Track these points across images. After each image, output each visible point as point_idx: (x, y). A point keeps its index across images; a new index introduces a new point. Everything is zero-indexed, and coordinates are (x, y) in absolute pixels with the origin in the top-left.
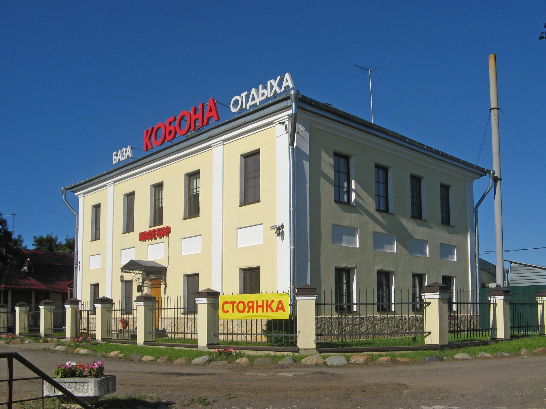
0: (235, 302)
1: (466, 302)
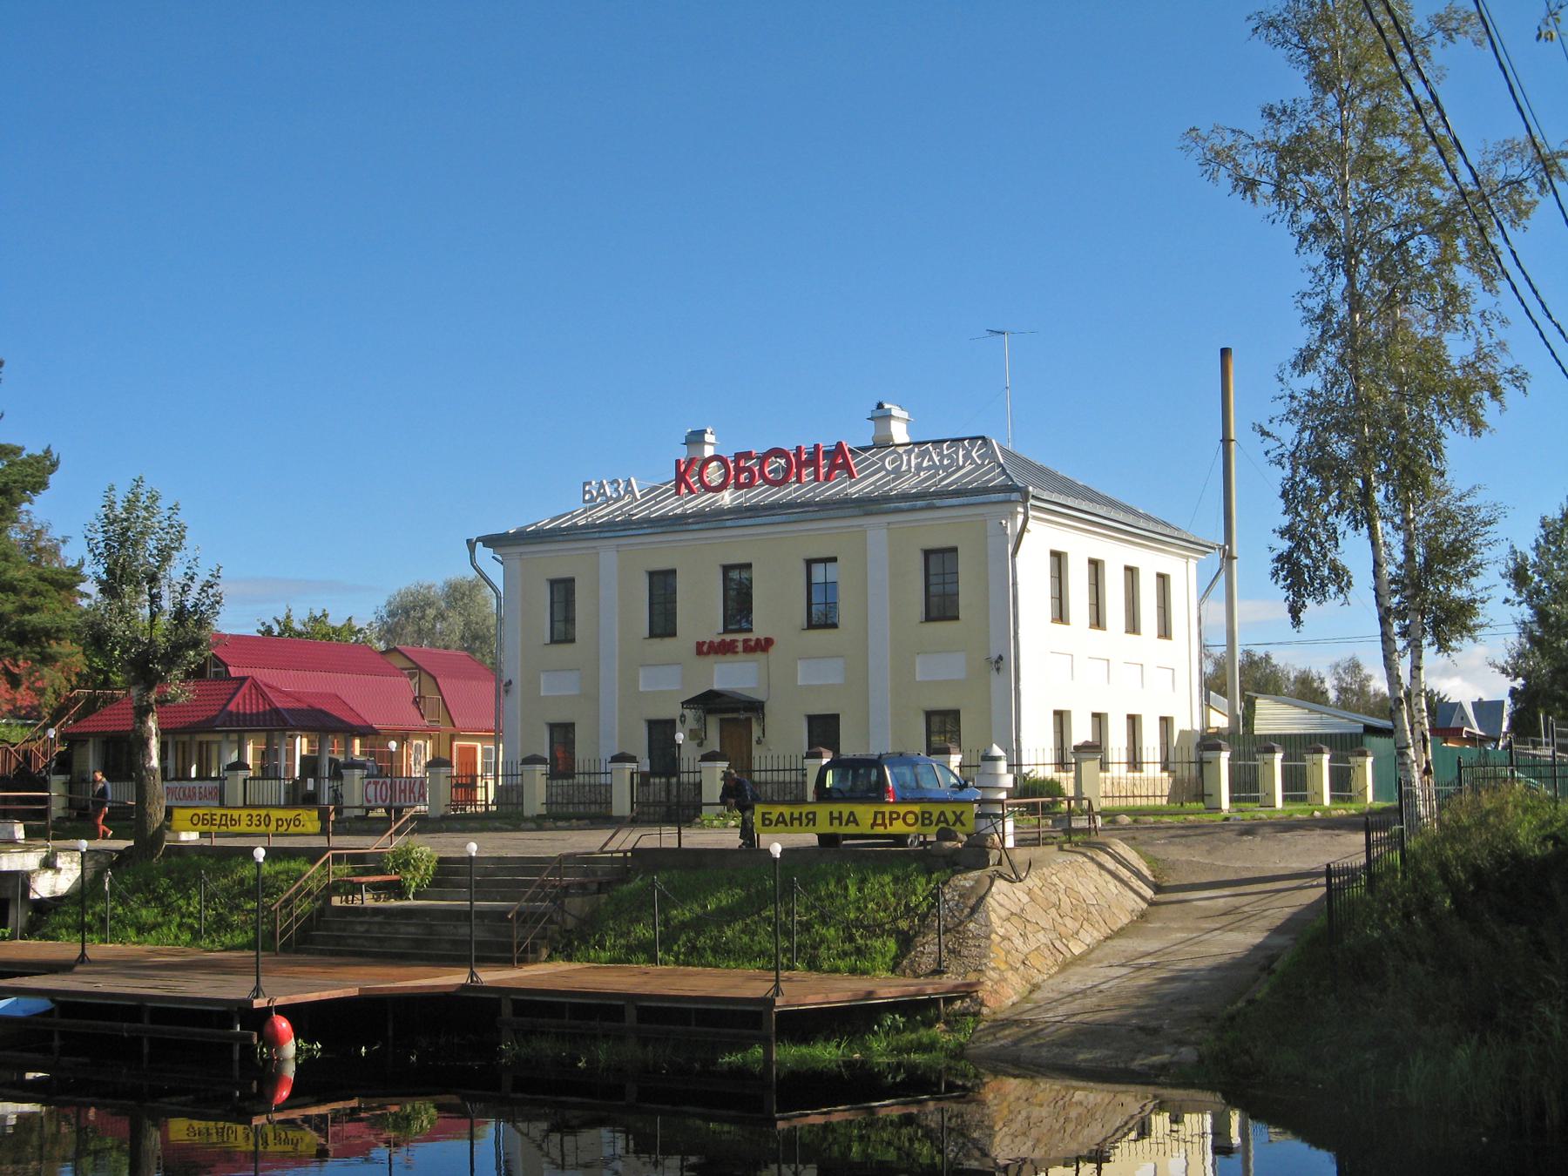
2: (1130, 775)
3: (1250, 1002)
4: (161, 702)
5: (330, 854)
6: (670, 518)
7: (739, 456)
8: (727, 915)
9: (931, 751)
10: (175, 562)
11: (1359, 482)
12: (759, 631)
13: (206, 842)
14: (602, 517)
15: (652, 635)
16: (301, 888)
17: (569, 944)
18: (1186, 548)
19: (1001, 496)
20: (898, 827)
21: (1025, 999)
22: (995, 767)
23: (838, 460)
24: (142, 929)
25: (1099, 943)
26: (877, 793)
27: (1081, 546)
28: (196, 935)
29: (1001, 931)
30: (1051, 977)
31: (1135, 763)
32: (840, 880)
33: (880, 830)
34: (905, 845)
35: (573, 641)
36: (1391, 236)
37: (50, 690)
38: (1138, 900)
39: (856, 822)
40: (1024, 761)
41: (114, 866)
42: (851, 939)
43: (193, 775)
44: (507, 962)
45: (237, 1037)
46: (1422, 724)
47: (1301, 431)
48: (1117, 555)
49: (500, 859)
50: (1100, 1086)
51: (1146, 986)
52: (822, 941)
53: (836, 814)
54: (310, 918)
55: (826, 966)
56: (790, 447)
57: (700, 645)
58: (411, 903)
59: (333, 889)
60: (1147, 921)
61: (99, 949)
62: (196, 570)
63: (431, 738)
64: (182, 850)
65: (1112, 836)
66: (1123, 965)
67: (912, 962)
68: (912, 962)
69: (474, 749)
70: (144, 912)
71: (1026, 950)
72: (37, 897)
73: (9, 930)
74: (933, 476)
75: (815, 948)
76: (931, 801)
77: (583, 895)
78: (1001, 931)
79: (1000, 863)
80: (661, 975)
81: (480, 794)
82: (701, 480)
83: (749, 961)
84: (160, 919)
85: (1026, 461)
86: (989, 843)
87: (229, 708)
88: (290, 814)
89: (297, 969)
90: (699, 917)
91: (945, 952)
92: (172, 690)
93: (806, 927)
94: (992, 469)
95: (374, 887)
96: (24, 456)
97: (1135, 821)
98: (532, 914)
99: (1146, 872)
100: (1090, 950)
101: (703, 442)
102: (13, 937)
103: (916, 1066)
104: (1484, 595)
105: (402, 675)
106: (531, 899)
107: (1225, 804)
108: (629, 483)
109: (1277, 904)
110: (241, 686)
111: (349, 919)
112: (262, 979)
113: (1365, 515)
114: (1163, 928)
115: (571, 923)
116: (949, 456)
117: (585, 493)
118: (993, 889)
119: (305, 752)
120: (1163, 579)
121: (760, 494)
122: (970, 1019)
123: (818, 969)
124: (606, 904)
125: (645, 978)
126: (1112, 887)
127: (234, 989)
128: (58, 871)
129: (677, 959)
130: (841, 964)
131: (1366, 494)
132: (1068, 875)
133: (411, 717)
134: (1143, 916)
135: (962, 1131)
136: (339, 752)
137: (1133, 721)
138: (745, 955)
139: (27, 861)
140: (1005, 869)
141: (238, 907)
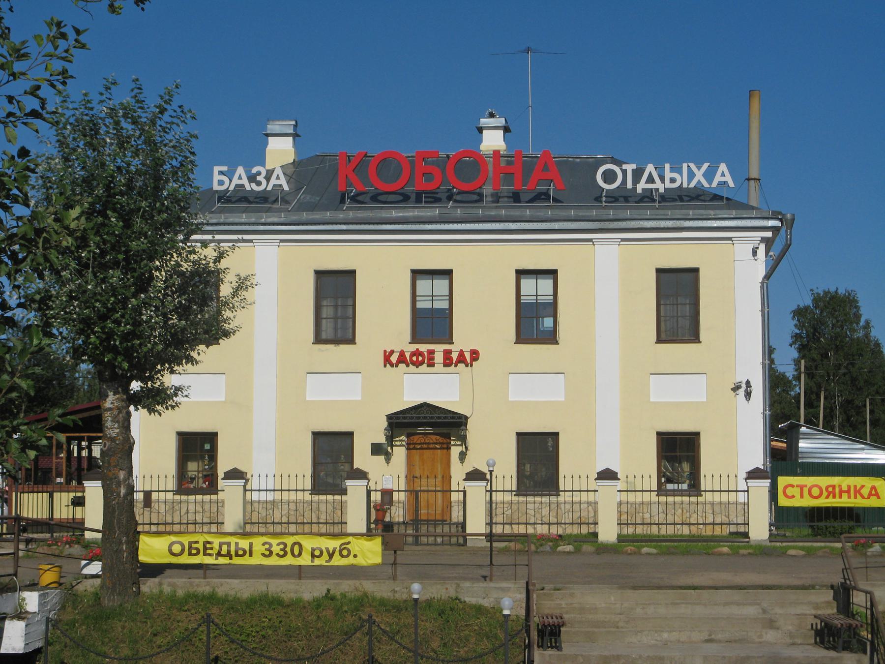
0: (806, 486)
1: (732, 488)
39: (877, 495)
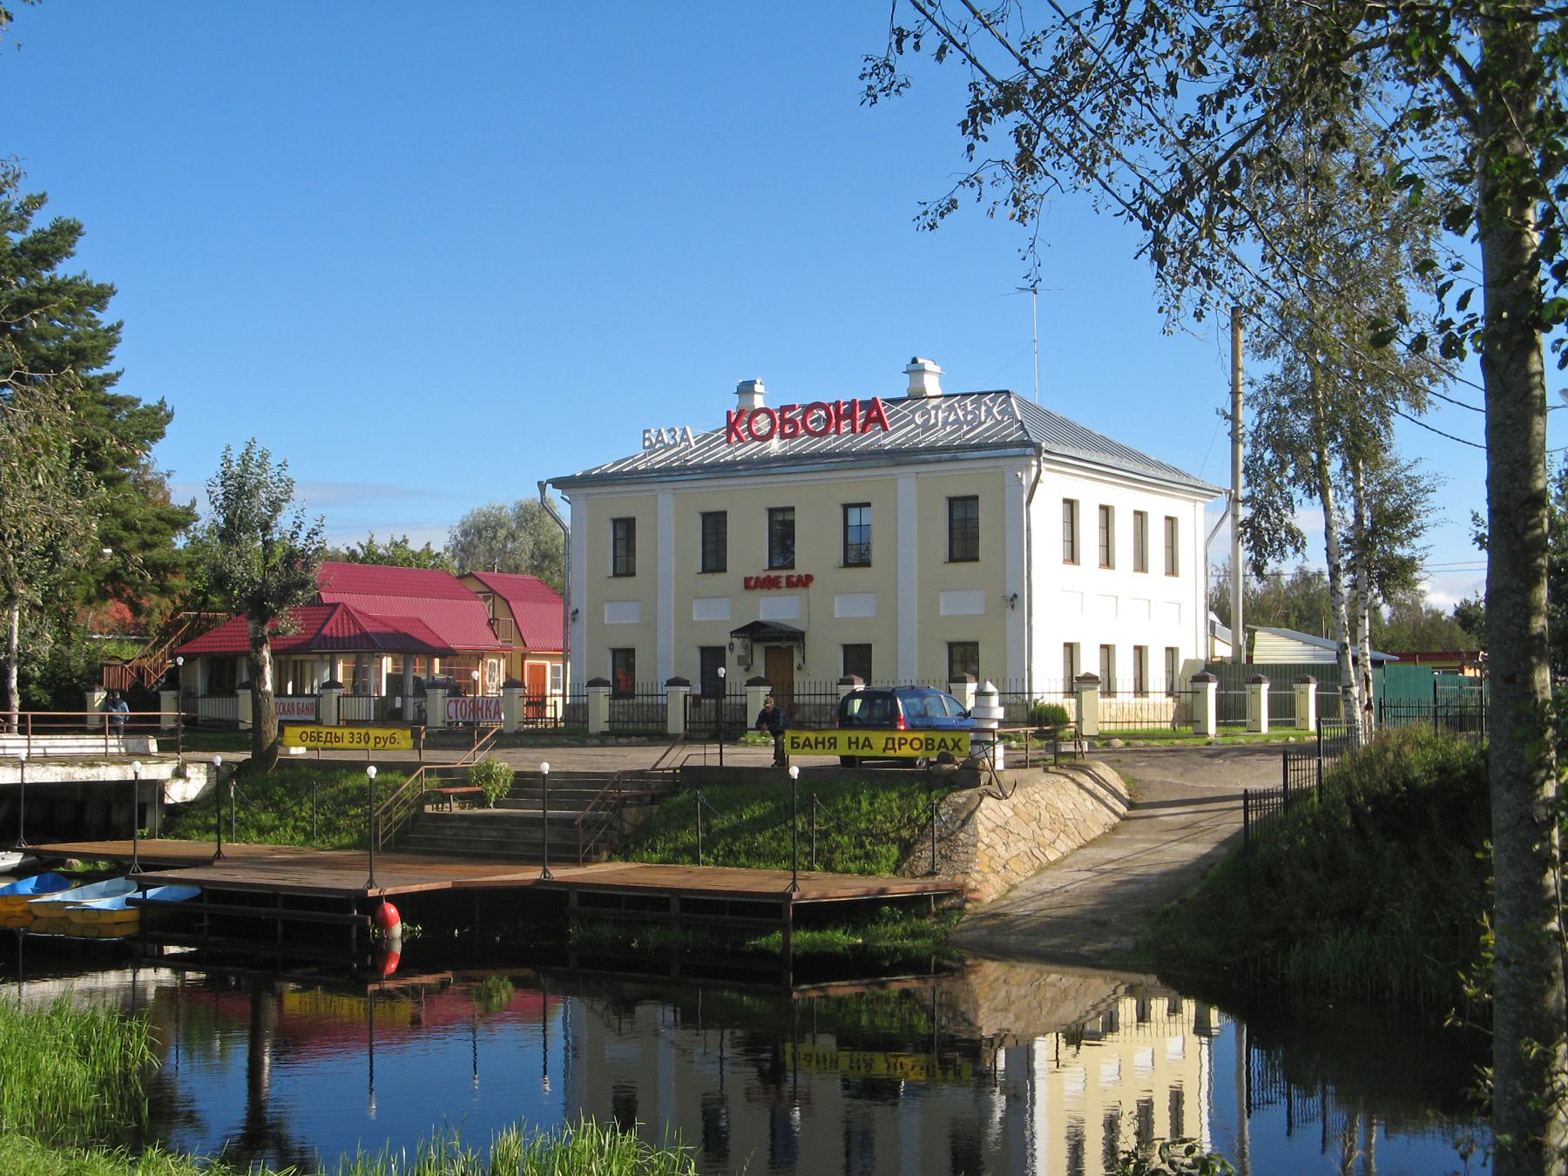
2: (1139, 700)
3: (1182, 901)
4: (274, 634)
5: (423, 768)
6: (721, 465)
7: (784, 409)
8: (759, 825)
9: (952, 679)
10: (284, 512)
11: (1314, 456)
12: (800, 569)
13: (313, 755)
14: (661, 461)
15: (705, 570)
16: (399, 798)
17: (626, 847)
18: (1194, 493)
19: (1017, 451)
20: (906, 751)
21: (1004, 897)
22: (988, 701)
23: (872, 413)
24: (262, 831)
25: (1073, 851)
26: (888, 721)
27: (1091, 493)
28: (309, 836)
29: (987, 841)
30: (1027, 879)
31: (1141, 690)
32: (855, 796)
33: (891, 753)
34: (914, 766)
35: (633, 574)
36: (1346, 239)
37: (157, 611)
38: (1112, 815)
40: (1034, 689)
41: (234, 775)
42: (862, 845)
43: (290, 692)
44: (575, 862)
45: (354, 919)
46: (1365, 666)
47: (1260, 413)
48: (1126, 500)
49: (568, 774)
50: (1070, 970)
51: (1105, 887)
52: (837, 847)
53: (853, 740)
54: (406, 824)
55: (839, 868)
56: (827, 399)
57: (747, 580)
58: (493, 811)
59: (426, 798)
60: (1117, 834)
61: (231, 848)
62: (303, 519)
63: (504, 656)
64: (294, 763)
65: (1099, 759)
66: (1089, 870)
67: (910, 866)
68: (910, 866)
69: (544, 667)
70: (263, 817)
71: (1007, 856)
72: (170, 802)
73: (147, 830)
74: (958, 430)
75: (832, 853)
76: (937, 728)
77: (639, 806)
78: (987, 841)
79: (990, 783)
80: (701, 874)
81: (549, 713)
82: (749, 429)
83: (776, 863)
84: (277, 823)
85: (1048, 414)
86: (980, 766)
87: (324, 632)
88: (385, 733)
89: (398, 866)
90: (735, 826)
91: (938, 858)
92: (283, 624)
93: (825, 835)
94: (1011, 425)
95: (460, 797)
96: (141, 407)
97: (1127, 745)
98: (595, 821)
99: (1123, 791)
100: (1064, 857)
101: (752, 392)
102: (151, 836)
103: (909, 950)
104: (1423, 553)
105: (477, 599)
106: (595, 809)
107: (1212, 728)
108: (684, 432)
109: (1230, 820)
110: (334, 610)
111: (439, 824)
112: (374, 874)
113: (1317, 484)
114: (1128, 840)
115: (627, 829)
116: (972, 412)
117: (645, 439)
118: (982, 805)
119: (390, 671)
120: (1171, 521)
121: (803, 444)
122: (956, 912)
123: (833, 870)
124: (658, 813)
125: (688, 876)
126: (1088, 803)
127: (352, 881)
128: (187, 780)
129: (716, 860)
130: (852, 866)
131: (1320, 467)
132: (1050, 794)
133: (486, 639)
134: (1115, 829)
135: (952, 1006)
136: (421, 670)
137: (1140, 651)
138: (774, 858)
139: (159, 771)
140: (994, 788)
141: (345, 814)
